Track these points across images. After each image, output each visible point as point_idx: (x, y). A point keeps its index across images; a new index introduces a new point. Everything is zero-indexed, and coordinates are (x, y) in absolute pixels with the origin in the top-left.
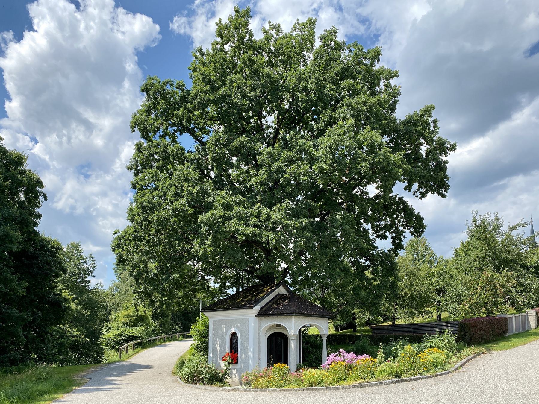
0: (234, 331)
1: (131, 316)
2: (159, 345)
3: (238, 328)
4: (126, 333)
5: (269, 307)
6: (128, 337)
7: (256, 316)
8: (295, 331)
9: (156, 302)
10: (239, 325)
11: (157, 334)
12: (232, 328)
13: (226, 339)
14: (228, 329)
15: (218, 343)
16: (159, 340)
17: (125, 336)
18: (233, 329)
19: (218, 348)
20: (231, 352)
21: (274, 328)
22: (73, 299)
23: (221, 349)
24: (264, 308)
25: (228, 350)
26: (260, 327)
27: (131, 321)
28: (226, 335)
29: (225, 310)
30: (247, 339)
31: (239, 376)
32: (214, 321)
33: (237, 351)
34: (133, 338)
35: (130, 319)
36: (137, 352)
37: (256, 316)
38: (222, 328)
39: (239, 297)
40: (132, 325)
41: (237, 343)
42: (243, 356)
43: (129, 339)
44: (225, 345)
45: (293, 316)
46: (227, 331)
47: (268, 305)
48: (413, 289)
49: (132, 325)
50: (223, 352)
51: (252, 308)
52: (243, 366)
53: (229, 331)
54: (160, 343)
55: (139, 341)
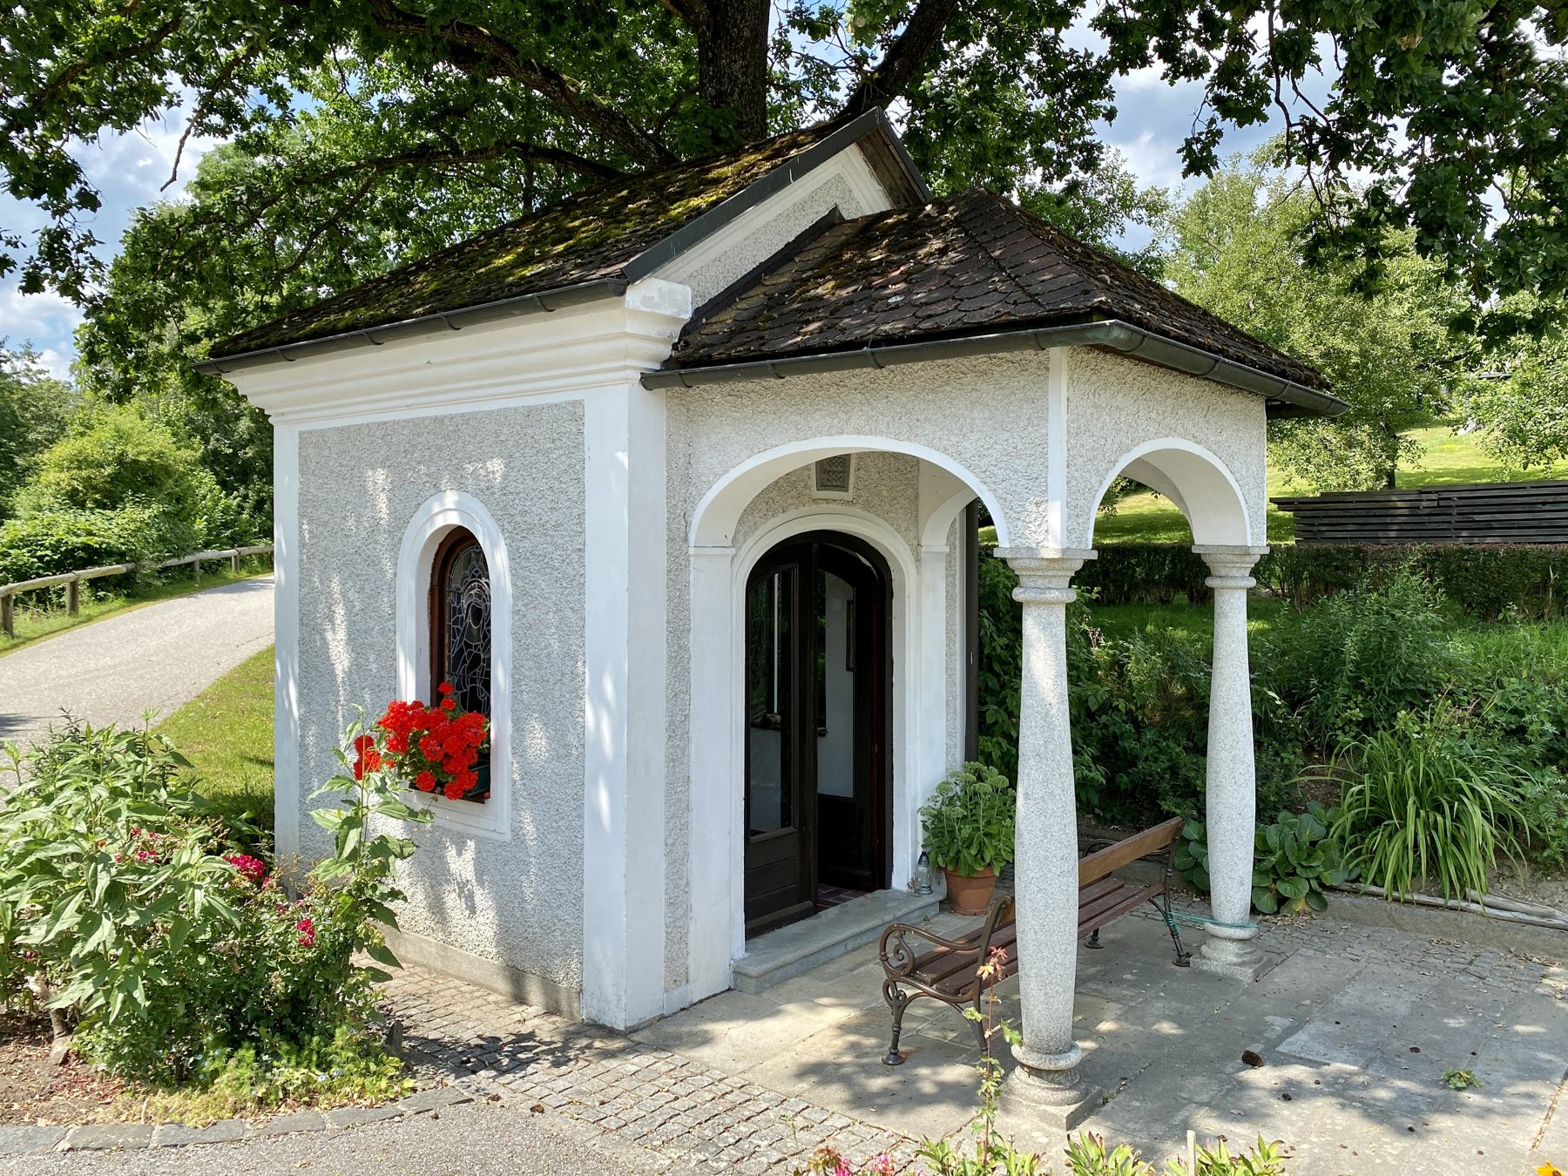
0: (454, 519)
1: (90, 465)
2: (237, 581)
3: (485, 492)
4: (59, 532)
5: (773, 303)
6: (70, 553)
7: (649, 381)
8: (1073, 512)
9: (238, 418)
10: (496, 466)
11: (234, 541)
12: (437, 489)
13: (392, 588)
14: (409, 500)
15: (340, 611)
16: (242, 562)
17: (55, 548)
18: (451, 498)
19: (340, 658)
20: (437, 697)
21: (801, 500)
22: (1008, 613)
23: (357, 666)
24: (728, 317)
25: (410, 686)
26: (687, 480)
27: (88, 483)
28: (395, 547)
29: (375, 340)
30: (573, 628)
31: (501, 911)
32: (305, 438)
33: (487, 685)
34: (93, 556)
35: (84, 473)
36: (89, 619)
37: (649, 381)
38: (364, 497)
39: (503, 247)
40: (96, 501)
41: (481, 615)
42: (538, 741)
43: (70, 559)
44: (389, 633)
45: (1058, 355)
46: (399, 523)
47: (757, 297)
48: (1362, 333)
49: (96, 501)
50: (377, 689)
51: (620, 285)
52: (529, 828)
53: (419, 517)
54: (244, 574)
55: (120, 569)
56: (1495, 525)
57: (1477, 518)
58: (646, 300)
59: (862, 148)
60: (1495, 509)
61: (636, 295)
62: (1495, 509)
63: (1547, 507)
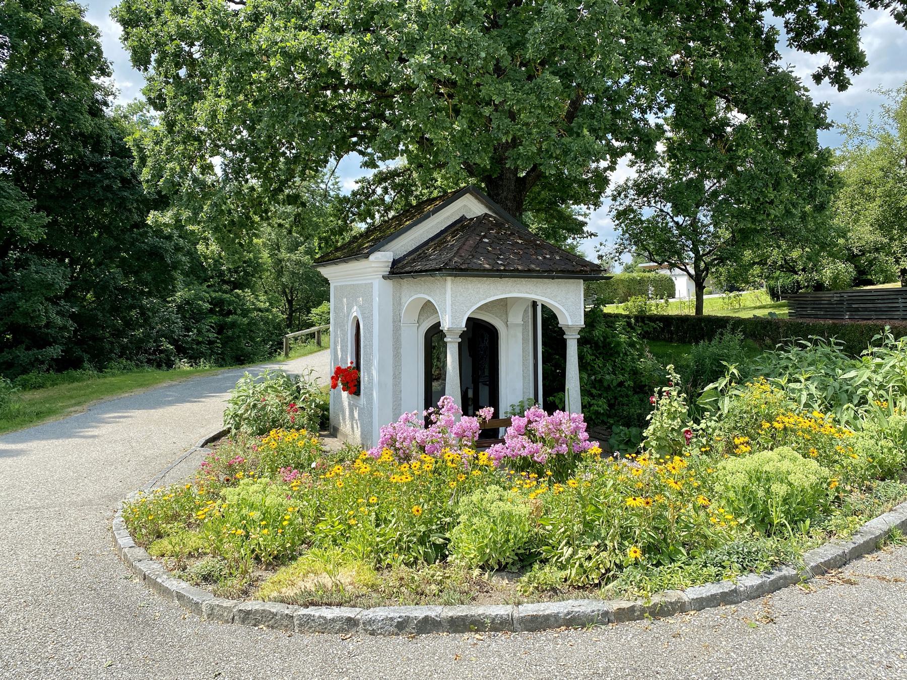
23: (342, 357)
56: (860, 309)
57: (854, 306)
58: (376, 258)
59: (471, 194)
60: (860, 302)
61: (372, 257)
62: (860, 302)
63: (879, 301)
